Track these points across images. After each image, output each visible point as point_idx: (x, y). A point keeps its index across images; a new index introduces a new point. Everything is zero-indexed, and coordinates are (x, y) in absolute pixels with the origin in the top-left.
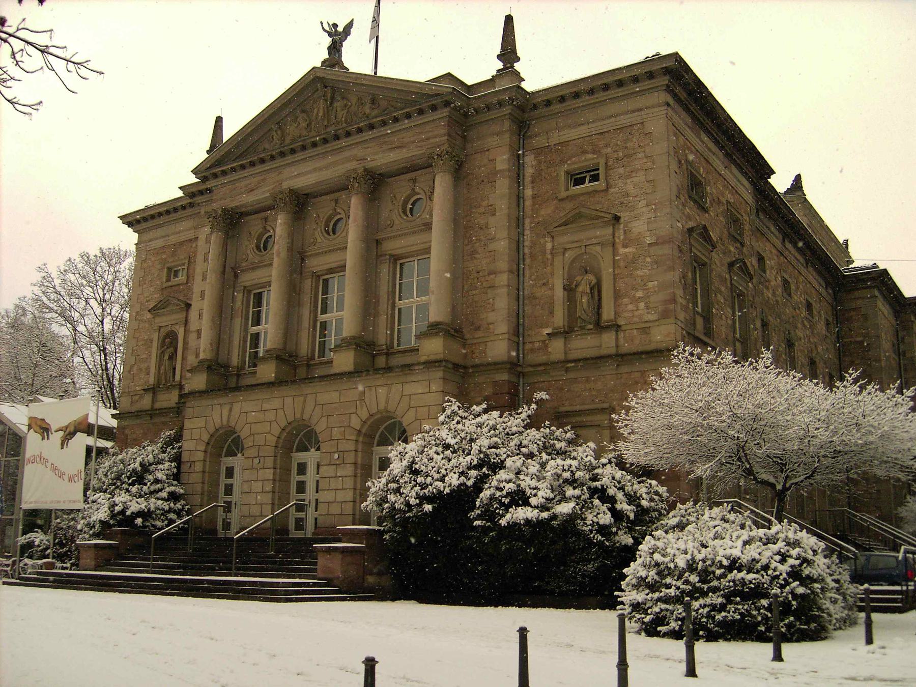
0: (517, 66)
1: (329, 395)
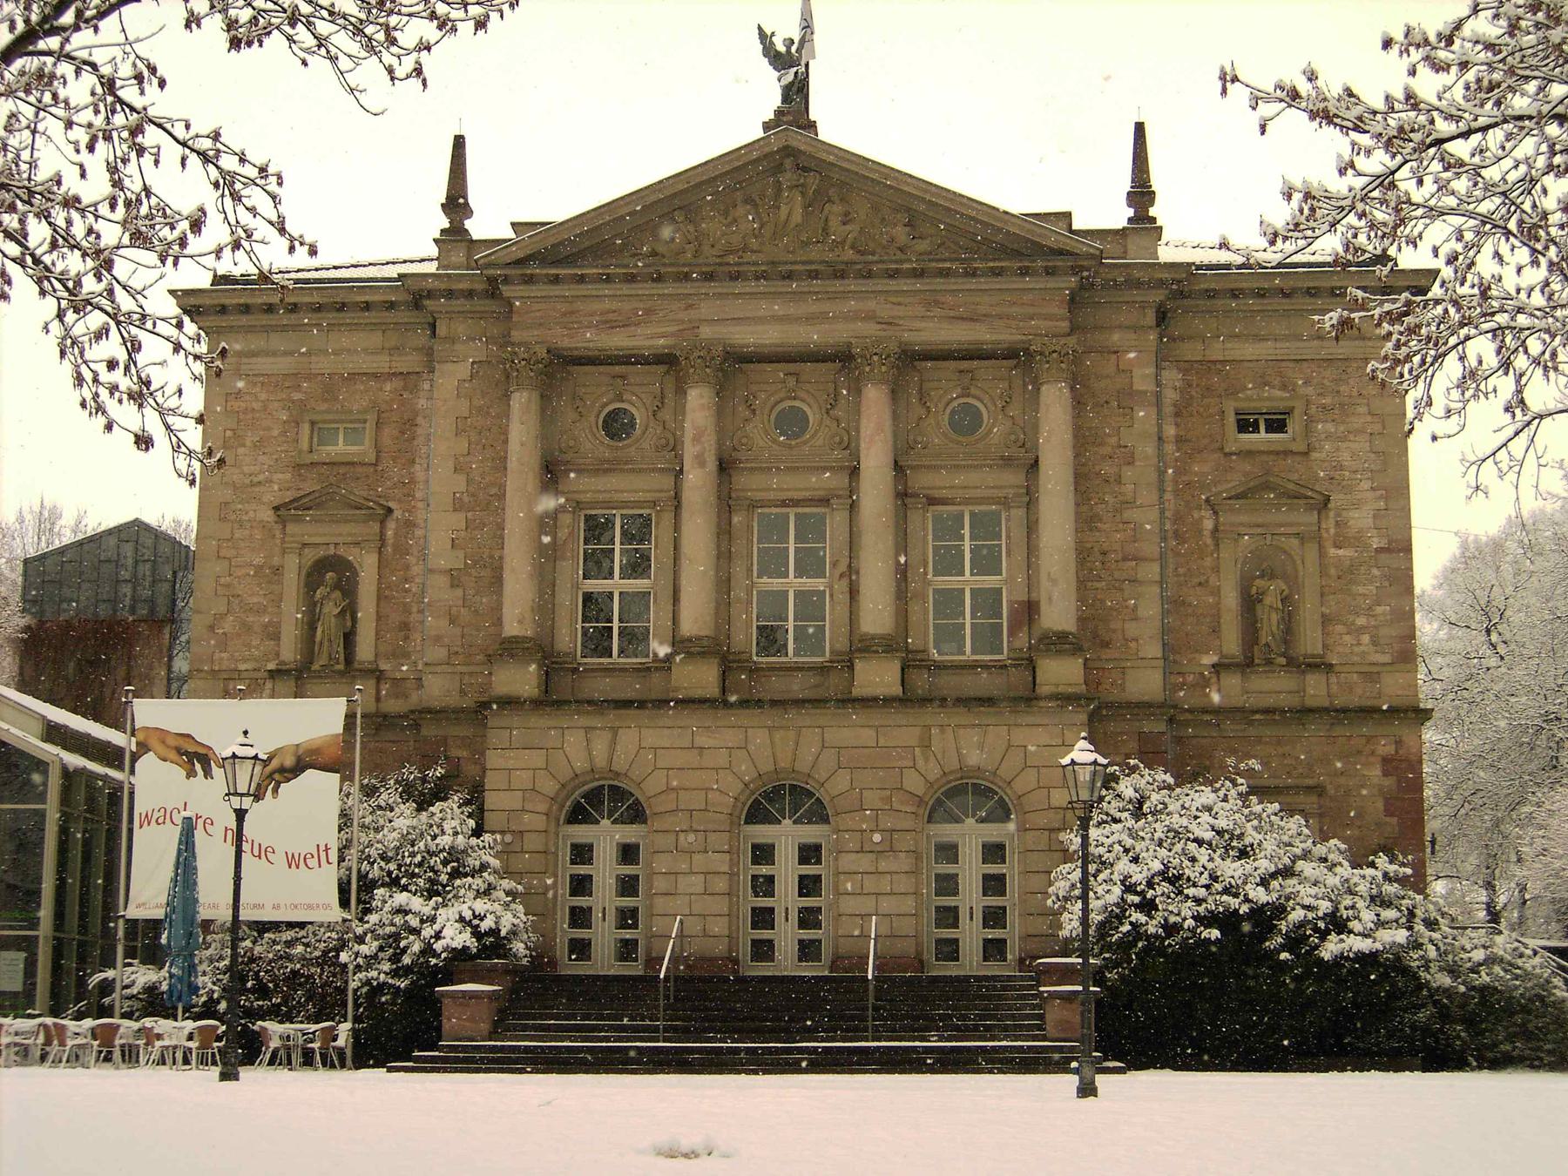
0: (1152, 212)
1: (853, 731)
